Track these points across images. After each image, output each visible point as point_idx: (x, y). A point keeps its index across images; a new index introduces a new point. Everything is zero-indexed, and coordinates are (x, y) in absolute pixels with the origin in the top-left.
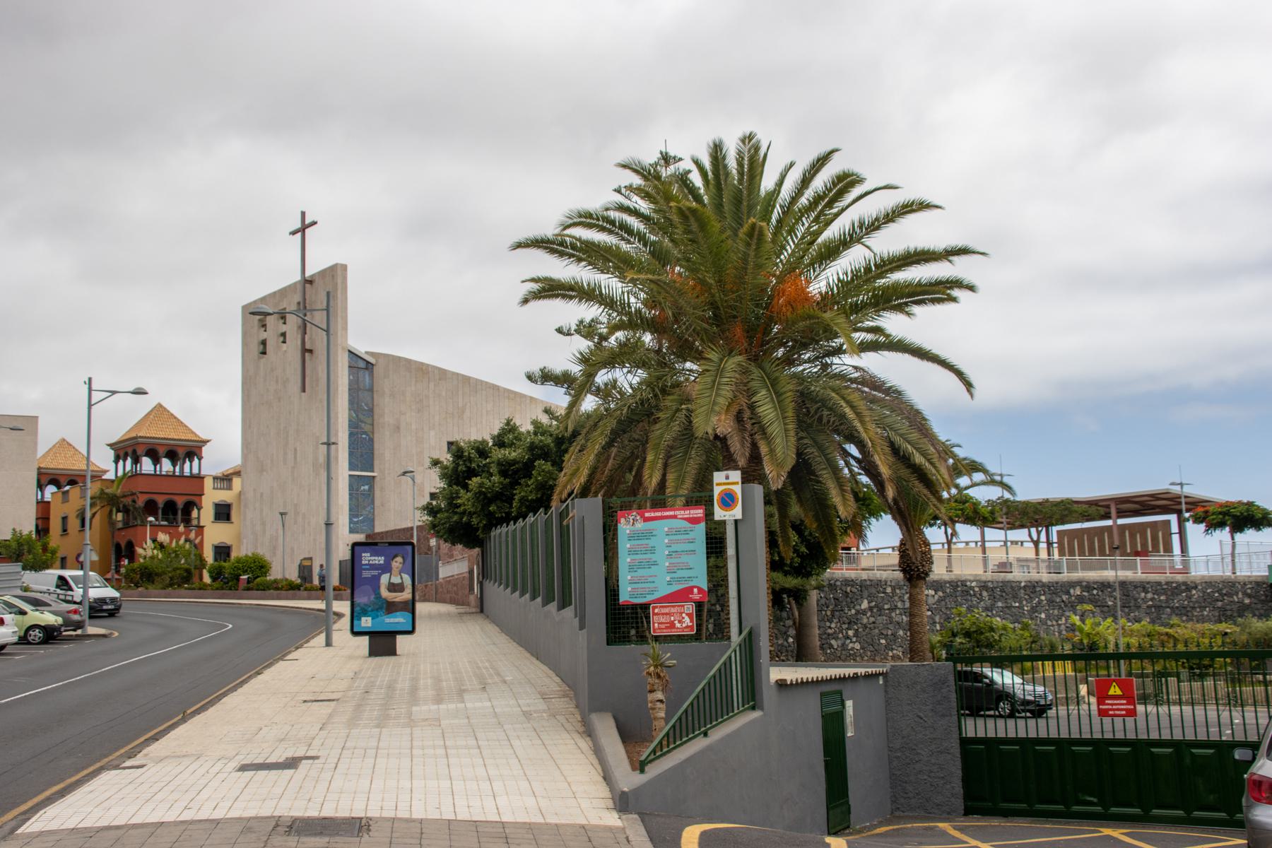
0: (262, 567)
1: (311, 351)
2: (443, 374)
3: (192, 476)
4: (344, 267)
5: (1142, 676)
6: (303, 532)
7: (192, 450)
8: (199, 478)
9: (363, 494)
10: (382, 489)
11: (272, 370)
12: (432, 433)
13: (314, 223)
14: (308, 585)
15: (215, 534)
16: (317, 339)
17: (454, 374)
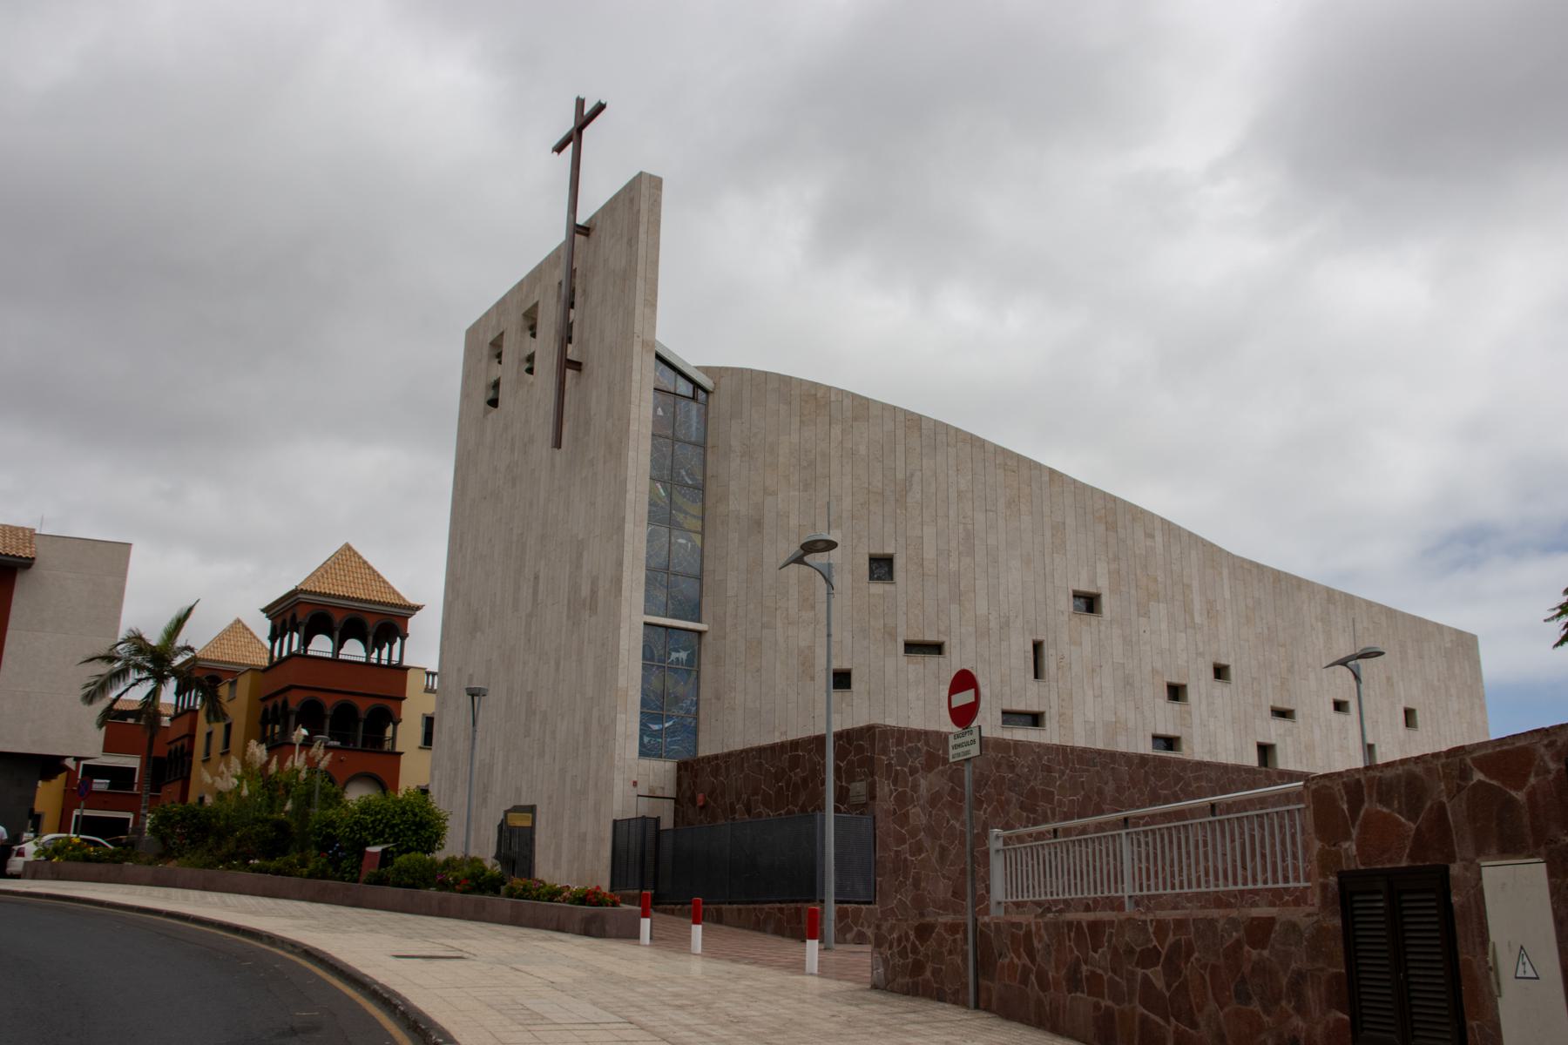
0: (422, 825)
1: (577, 366)
3: (390, 666)
4: (656, 183)
5: (919, 902)
7: (385, 623)
8: (401, 670)
13: (600, 108)
15: (415, 770)
17: (884, 406)
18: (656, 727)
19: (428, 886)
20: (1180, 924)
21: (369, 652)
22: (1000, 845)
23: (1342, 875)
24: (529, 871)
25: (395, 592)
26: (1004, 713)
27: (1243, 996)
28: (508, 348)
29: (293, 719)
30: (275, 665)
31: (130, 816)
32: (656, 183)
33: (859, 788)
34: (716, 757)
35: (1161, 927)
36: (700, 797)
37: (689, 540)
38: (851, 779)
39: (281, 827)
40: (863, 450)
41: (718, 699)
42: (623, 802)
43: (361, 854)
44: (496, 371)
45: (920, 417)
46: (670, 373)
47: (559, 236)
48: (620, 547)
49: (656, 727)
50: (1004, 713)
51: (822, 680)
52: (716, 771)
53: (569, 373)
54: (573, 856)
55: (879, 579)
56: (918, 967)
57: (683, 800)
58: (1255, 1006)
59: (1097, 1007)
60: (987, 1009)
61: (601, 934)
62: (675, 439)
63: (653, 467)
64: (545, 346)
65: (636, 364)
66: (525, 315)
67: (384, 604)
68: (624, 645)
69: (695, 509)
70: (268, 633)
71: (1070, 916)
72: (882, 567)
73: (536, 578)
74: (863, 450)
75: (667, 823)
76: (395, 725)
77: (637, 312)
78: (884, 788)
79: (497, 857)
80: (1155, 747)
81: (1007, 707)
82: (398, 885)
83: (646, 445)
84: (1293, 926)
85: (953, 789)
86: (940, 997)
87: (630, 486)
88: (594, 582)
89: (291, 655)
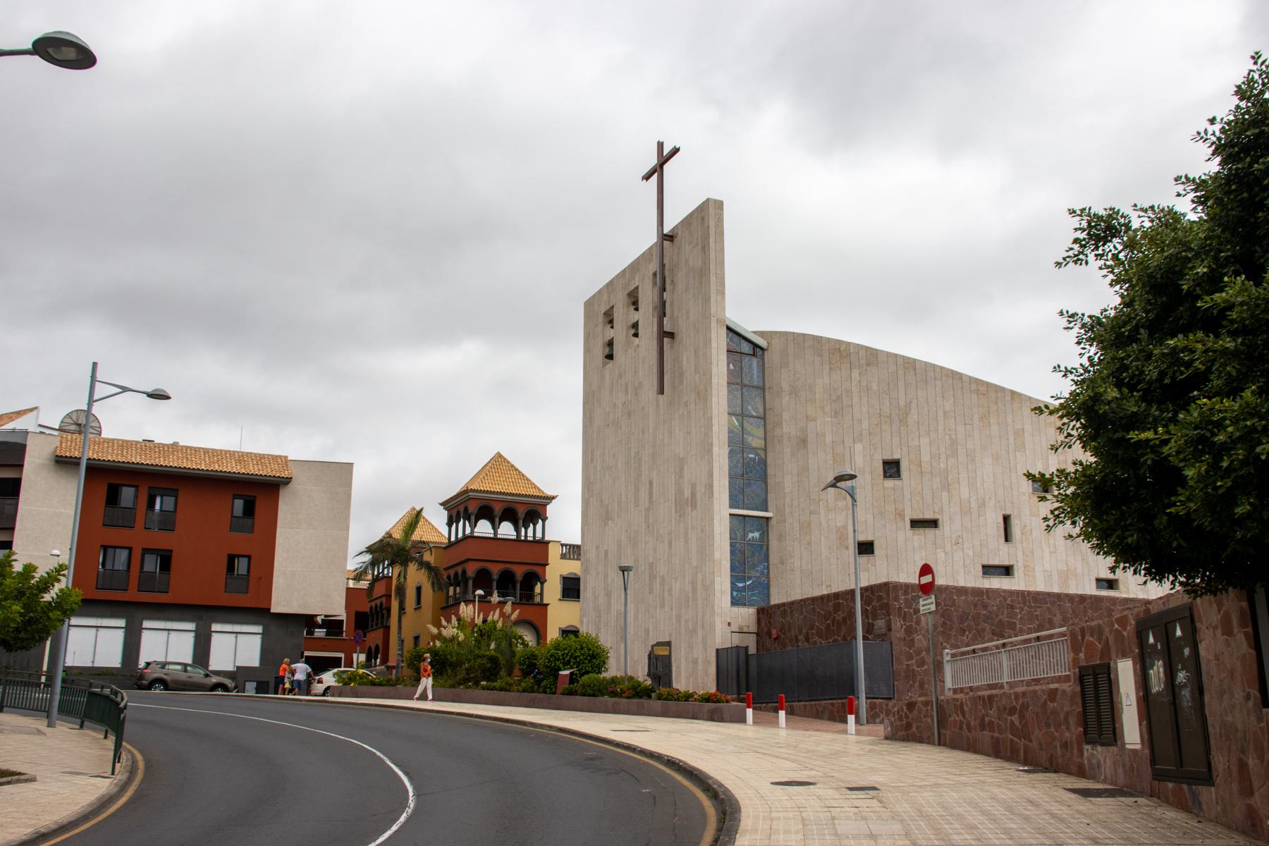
0: (594, 656)
1: (671, 335)
2: (872, 356)
3: (535, 542)
4: (719, 205)
6: (662, 605)
7: (530, 510)
8: (543, 544)
9: (751, 558)
10: (781, 538)
11: (620, 376)
12: (859, 447)
13: (675, 151)
14: (663, 690)
15: (560, 615)
16: (682, 317)
18: (741, 585)
19: (603, 695)
20: (1024, 693)
21: (517, 530)
22: (948, 658)
23: (1081, 668)
24: (669, 684)
25: (536, 487)
26: (984, 567)
27: (1048, 725)
28: (618, 316)
29: (470, 583)
30: (451, 545)
31: (342, 655)
32: (719, 205)
33: (880, 624)
34: (784, 604)
35: (1017, 695)
36: (774, 631)
37: (757, 454)
38: (875, 617)
39: (493, 660)
40: (875, 386)
41: (782, 563)
42: (722, 637)
43: (556, 676)
44: (610, 334)
45: (915, 361)
46: (736, 338)
47: (653, 239)
48: (710, 463)
49: (741, 585)
50: (984, 567)
51: (852, 548)
52: (784, 614)
53: (666, 340)
54: (694, 673)
55: (891, 476)
56: (909, 726)
57: (763, 631)
58: (1052, 729)
59: (992, 737)
60: (945, 745)
61: (721, 719)
62: (743, 386)
63: (729, 406)
64: (646, 316)
65: (714, 336)
66: (629, 295)
67: (529, 496)
68: (717, 530)
69: (760, 432)
70: (445, 520)
71: (980, 693)
72: (892, 468)
73: (651, 483)
74: (875, 386)
75: (752, 650)
76: (542, 584)
77: (712, 299)
78: (897, 623)
79: (649, 675)
80: (1098, 587)
81: (986, 563)
82: (584, 695)
83: (724, 391)
84: (1064, 691)
85: (944, 623)
86: (920, 740)
87: (715, 422)
88: (693, 487)
89: (465, 538)
